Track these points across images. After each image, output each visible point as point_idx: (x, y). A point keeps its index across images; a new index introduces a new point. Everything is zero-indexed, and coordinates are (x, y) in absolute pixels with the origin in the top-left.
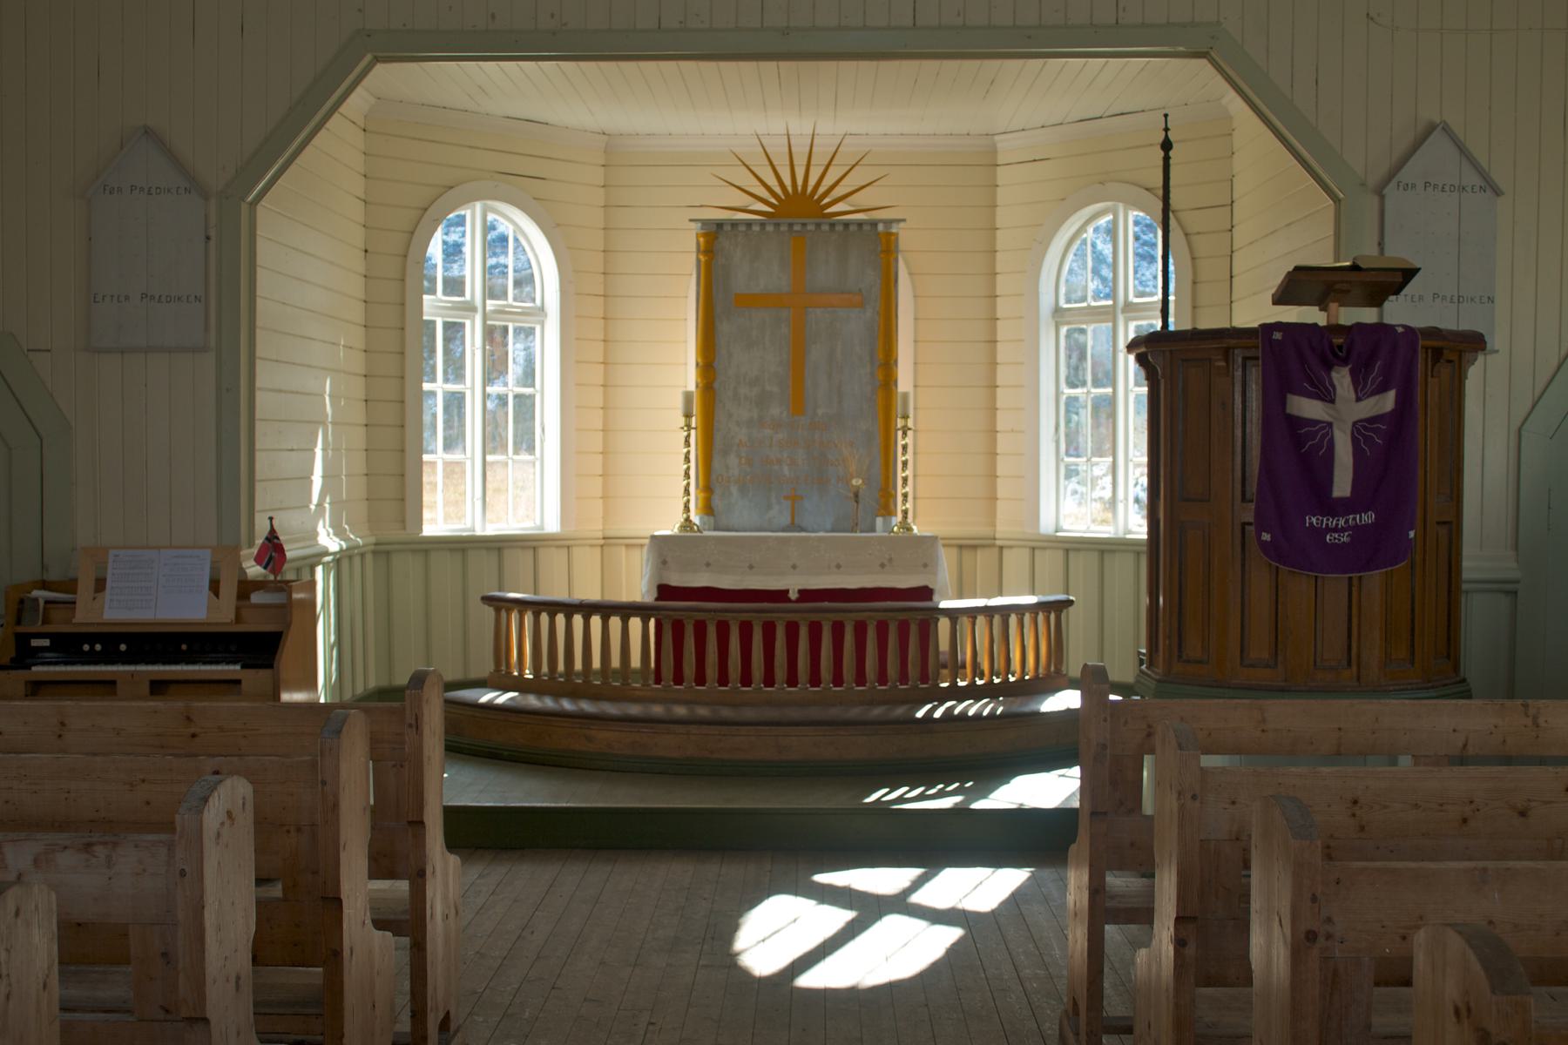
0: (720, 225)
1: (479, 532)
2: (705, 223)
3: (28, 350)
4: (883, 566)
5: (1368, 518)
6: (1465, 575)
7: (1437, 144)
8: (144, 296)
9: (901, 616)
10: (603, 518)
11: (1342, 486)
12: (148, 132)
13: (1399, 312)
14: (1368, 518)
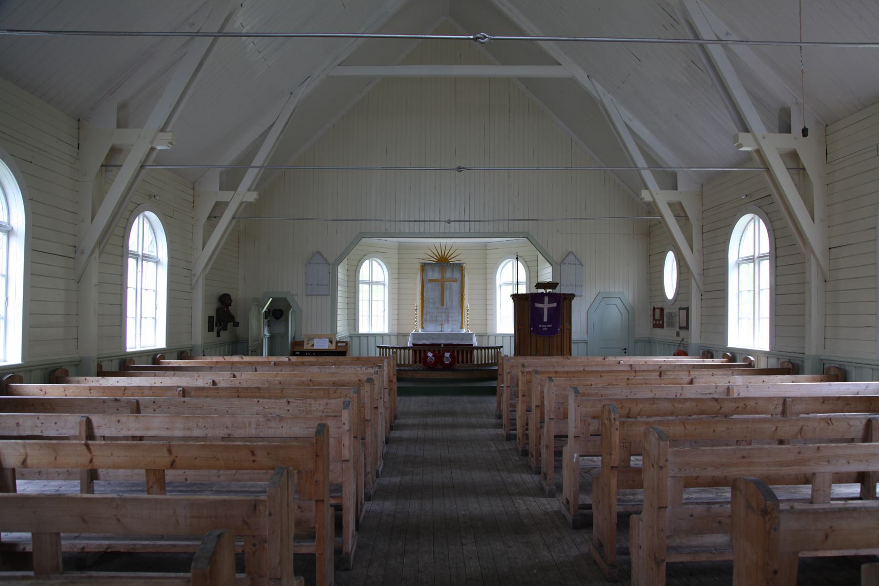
0: (425, 264)
1: (370, 332)
2: (422, 263)
3: (824, 364)
4: (462, 339)
5: (551, 326)
6: (572, 339)
7: (571, 257)
8: (317, 284)
9: (467, 349)
10: (320, 338)
11: (545, 319)
12: (318, 252)
13: (557, 291)
14: (551, 326)
